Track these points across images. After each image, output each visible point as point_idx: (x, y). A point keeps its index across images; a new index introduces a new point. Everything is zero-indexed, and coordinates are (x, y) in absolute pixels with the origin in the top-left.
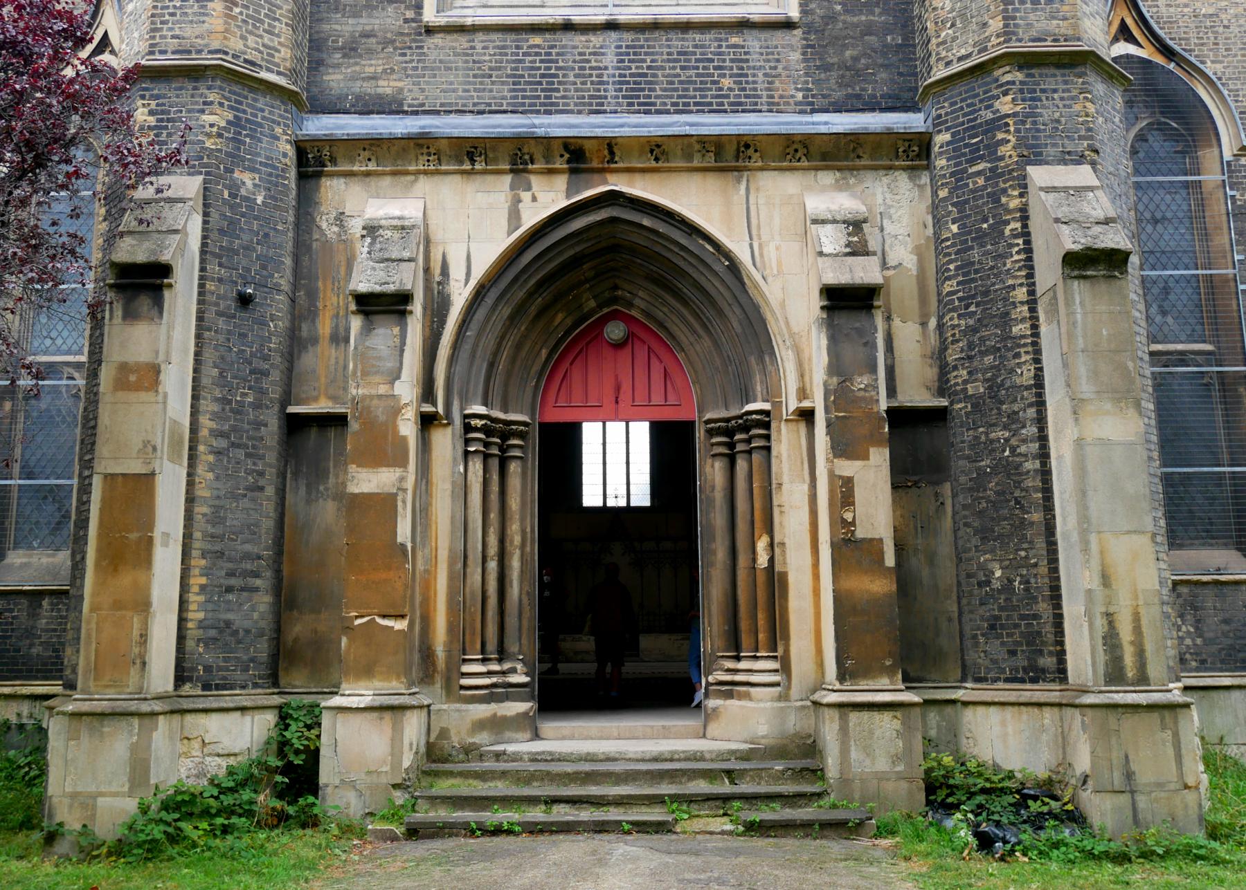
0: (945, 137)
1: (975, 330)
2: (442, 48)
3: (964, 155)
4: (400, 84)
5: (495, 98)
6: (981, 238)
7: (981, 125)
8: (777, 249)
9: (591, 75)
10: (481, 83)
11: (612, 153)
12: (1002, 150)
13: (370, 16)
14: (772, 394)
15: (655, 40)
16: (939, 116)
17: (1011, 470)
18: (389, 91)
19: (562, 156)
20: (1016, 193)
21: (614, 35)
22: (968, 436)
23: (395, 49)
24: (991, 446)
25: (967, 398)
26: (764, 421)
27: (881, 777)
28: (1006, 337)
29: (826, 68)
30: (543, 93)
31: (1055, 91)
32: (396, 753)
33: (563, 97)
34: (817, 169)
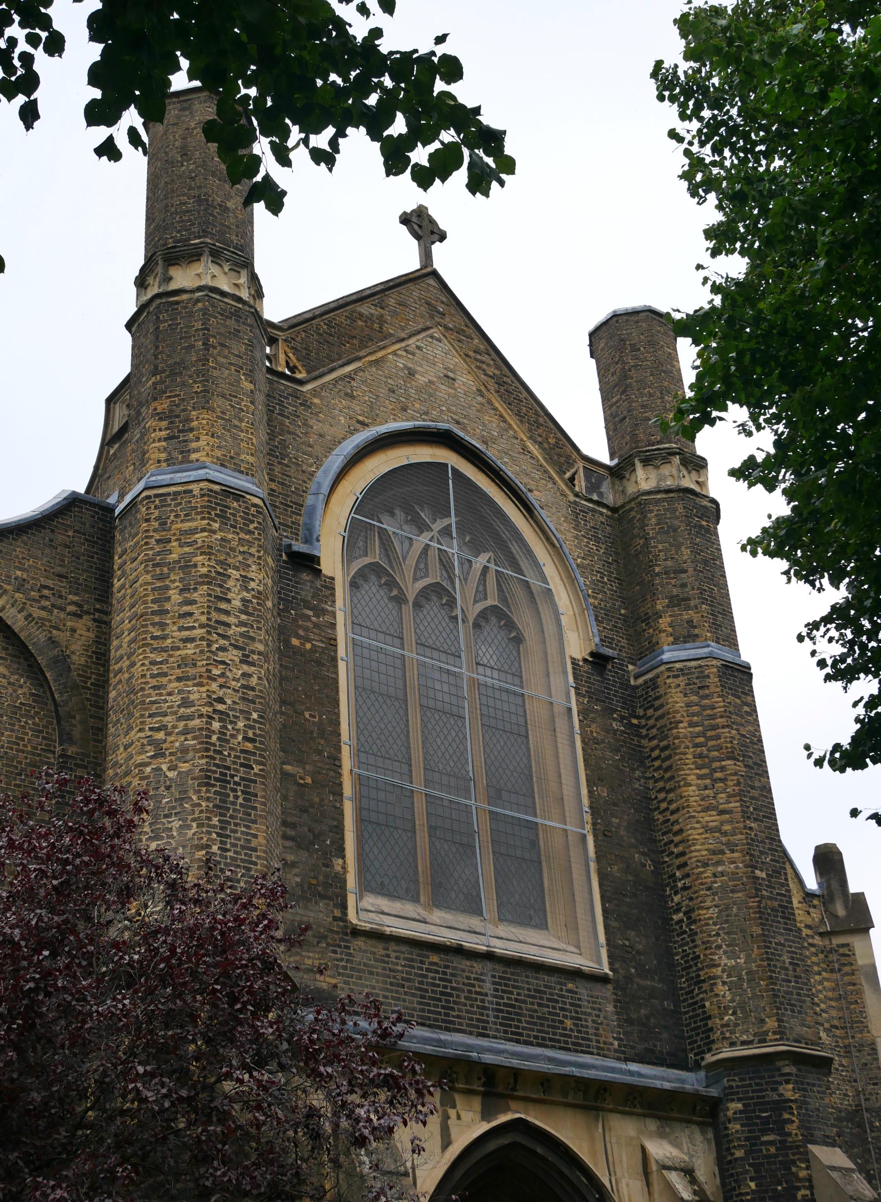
0: (736, 1106)
2: (365, 951)
3: (757, 1124)
4: (334, 981)
5: (407, 1008)
7: (768, 1103)
8: (628, 1185)
9: (476, 1000)
10: (397, 992)
11: (516, 1081)
13: (306, 908)
15: (518, 975)
16: (731, 1087)
18: (325, 986)
19: (479, 1079)
20: (803, 1165)
21: (489, 965)
23: (328, 944)
29: (630, 1021)
31: (814, 1085)
33: (458, 1017)
34: (645, 1116)
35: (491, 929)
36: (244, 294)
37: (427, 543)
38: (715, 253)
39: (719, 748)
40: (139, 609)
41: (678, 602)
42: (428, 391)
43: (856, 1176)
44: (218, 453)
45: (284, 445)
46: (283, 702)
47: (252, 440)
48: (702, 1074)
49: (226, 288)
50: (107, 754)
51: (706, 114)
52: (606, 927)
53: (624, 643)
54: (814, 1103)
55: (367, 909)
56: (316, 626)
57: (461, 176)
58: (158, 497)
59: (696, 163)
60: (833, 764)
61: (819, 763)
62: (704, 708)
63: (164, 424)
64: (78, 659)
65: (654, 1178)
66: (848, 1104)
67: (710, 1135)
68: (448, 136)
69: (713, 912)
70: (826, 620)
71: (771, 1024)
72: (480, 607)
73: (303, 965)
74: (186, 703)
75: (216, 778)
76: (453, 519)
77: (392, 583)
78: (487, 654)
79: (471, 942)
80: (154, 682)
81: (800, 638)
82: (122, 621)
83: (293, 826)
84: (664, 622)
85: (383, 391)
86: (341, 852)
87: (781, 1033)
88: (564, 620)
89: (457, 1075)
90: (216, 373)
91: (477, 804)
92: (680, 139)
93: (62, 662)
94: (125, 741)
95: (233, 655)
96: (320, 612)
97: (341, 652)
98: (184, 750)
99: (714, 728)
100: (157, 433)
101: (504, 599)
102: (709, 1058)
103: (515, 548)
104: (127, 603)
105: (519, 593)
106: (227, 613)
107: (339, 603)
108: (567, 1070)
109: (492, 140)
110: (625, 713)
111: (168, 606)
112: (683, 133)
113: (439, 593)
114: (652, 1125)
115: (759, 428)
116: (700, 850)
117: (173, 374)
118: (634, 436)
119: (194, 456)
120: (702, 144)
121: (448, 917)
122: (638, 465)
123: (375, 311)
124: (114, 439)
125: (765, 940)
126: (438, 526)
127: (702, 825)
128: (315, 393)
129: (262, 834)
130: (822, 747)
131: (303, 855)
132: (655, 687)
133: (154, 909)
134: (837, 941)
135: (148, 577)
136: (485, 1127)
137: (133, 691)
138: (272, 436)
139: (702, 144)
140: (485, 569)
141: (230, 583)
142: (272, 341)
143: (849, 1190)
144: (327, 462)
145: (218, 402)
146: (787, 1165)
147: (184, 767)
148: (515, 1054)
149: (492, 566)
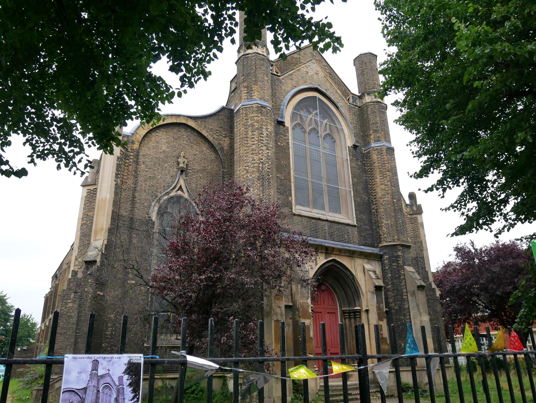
1: (396, 296)
6: (396, 278)
12: (399, 262)
14: (360, 306)
17: (405, 324)
21: (327, 222)
22: (395, 317)
24: (400, 320)
25: (395, 310)
26: (359, 311)
27: (392, 386)
28: (402, 298)
29: (361, 236)
30: (315, 234)
32: (316, 386)
35: (327, 214)
36: (265, 54)
37: (312, 117)
38: (389, 46)
39: (385, 169)
40: (241, 136)
41: (376, 131)
42: (311, 77)
43: (415, 273)
44: (260, 96)
45: (275, 93)
46: (276, 159)
47: (268, 92)
48: (378, 249)
49: (260, 53)
50: (234, 172)
51: (388, 13)
52: (356, 213)
53: (361, 142)
54: (406, 256)
55: (297, 209)
56: (284, 139)
57: (331, 50)
58: (245, 108)
59: (386, 27)
60: (414, 177)
61: (411, 177)
62: (382, 159)
63: (246, 89)
64: (226, 148)
65: (366, 273)
66: (415, 256)
67: (380, 263)
68: (328, 40)
69: (382, 210)
70: (414, 141)
71: (396, 237)
72: (325, 133)
73: (284, 224)
74: (253, 160)
75: (261, 178)
76: (318, 111)
77: (303, 128)
78: (327, 145)
79: (322, 217)
80: (245, 155)
81: (407, 145)
82: (237, 139)
83: (279, 189)
84: (372, 137)
85: (300, 78)
86: (291, 195)
87: (398, 239)
88: (346, 136)
89: (318, 248)
90: (258, 75)
91: (324, 183)
92: (381, 20)
93: (222, 149)
94: (239, 169)
95: (264, 148)
96: (285, 136)
97: (290, 146)
98: (253, 171)
99: (384, 164)
100: (244, 91)
101: (331, 131)
102: (380, 245)
103: (334, 118)
104: (238, 135)
105: (335, 130)
106: (263, 137)
107: (290, 133)
108: (346, 248)
109: (338, 40)
110: (361, 160)
111: (248, 136)
112: (381, 18)
113: (315, 130)
114: (366, 261)
115: (399, 92)
116: (379, 195)
117: (248, 76)
118: (365, 88)
119: (253, 97)
120: (387, 21)
121: (317, 211)
122: (366, 95)
123: (298, 56)
124: (233, 92)
125: (395, 217)
126: (314, 112)
127: (380, 189)
128: (283, 79)
129: (273, 192)
130: (412, 173)
131: (282, 196)
132: (369, 153)
133: (248, 210)
134: (414, 216)
135: (243, 129)
136: (326, 261)
137: (240, 157)
138: (272, 91)
139: (387, 21)
140: (326, 124)
141: (263, 130)
142: (272, 65)
143: (414, 277)
144: (286, 97)
145: (259, 83)
146: (399, 271)
147: (253, 176)
148: (333, 244)
149: (328, 123)
